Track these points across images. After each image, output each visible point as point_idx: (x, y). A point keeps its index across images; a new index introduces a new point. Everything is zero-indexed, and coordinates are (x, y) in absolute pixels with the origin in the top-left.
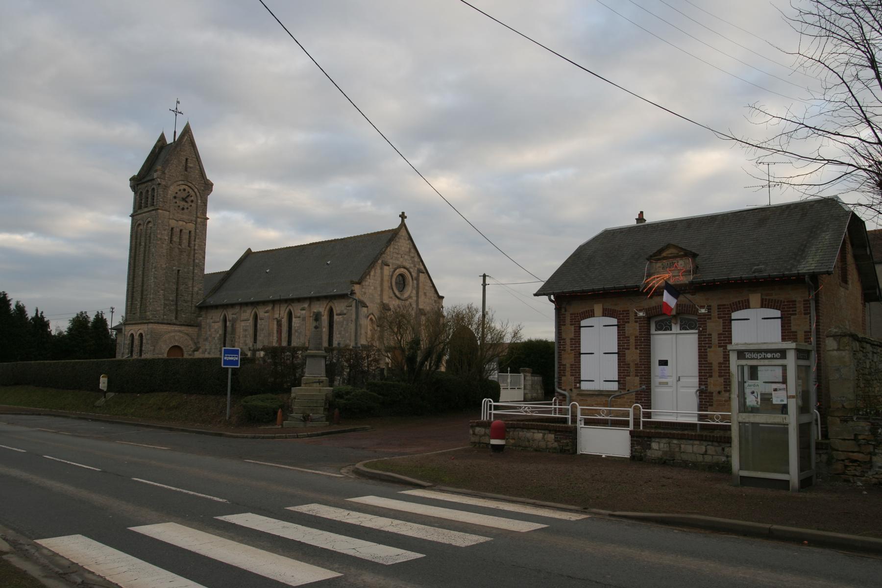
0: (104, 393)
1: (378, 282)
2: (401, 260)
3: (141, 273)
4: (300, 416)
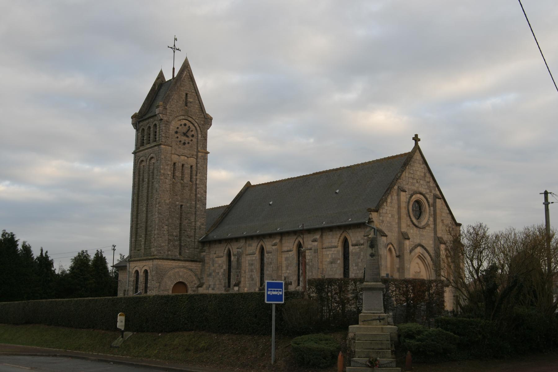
0: (122, 332)
1: (395, 209)
2: (417, 185)
3: (144, 209)
4: (364, 360)
